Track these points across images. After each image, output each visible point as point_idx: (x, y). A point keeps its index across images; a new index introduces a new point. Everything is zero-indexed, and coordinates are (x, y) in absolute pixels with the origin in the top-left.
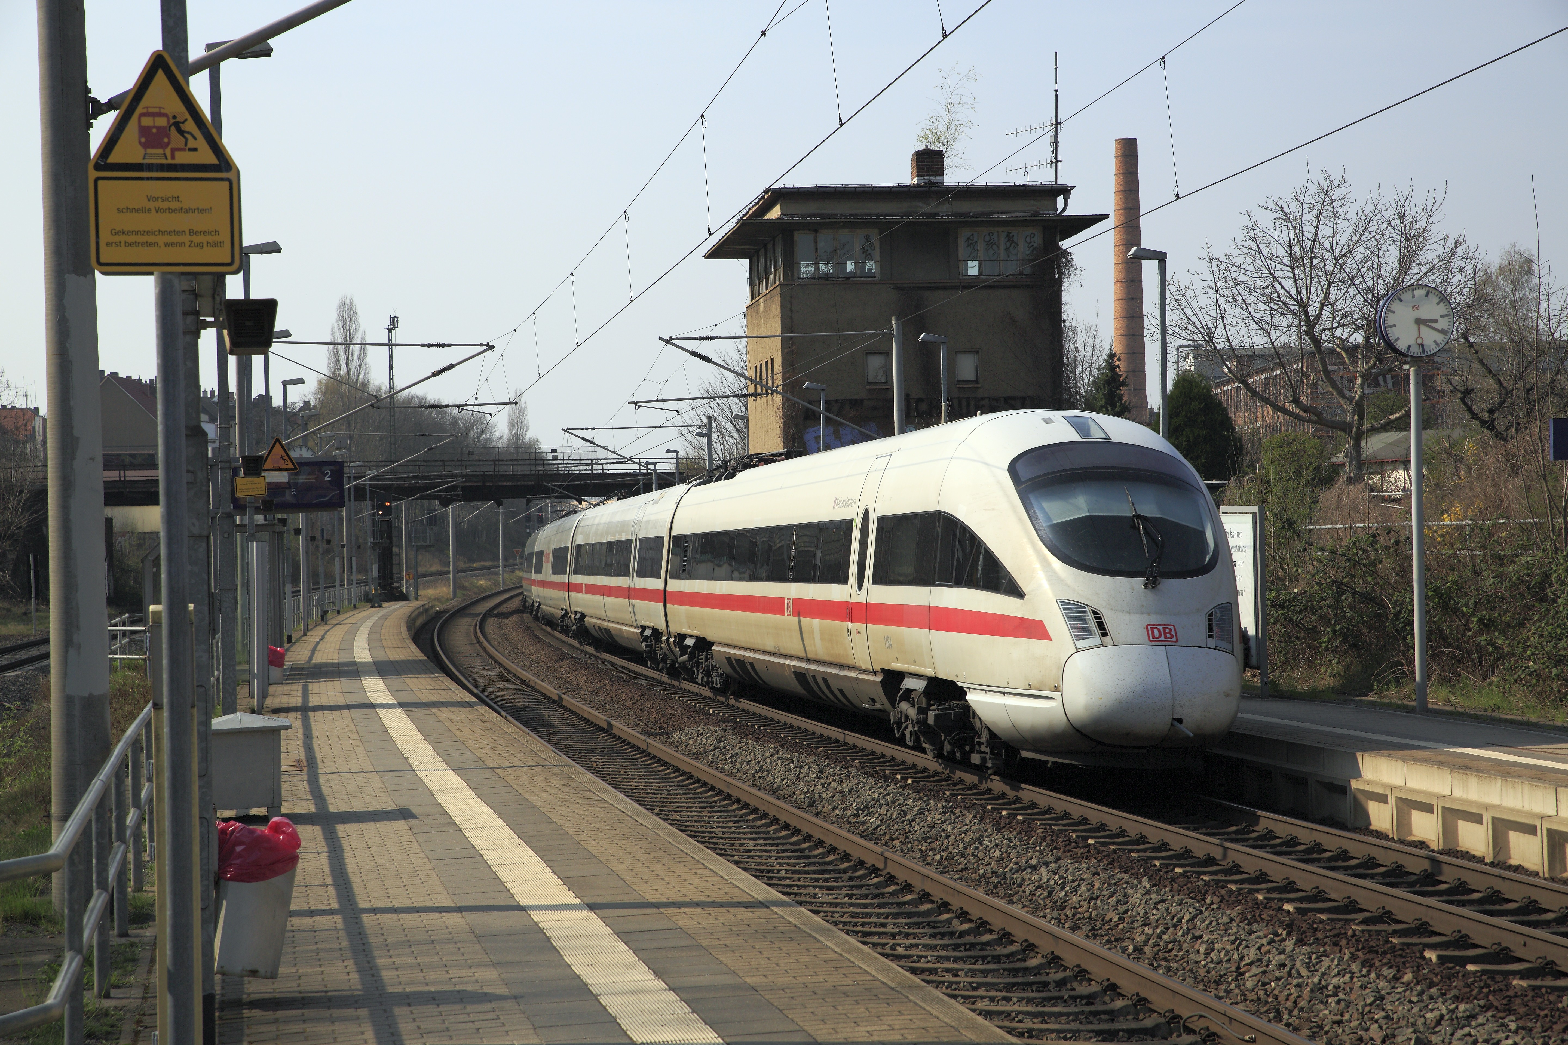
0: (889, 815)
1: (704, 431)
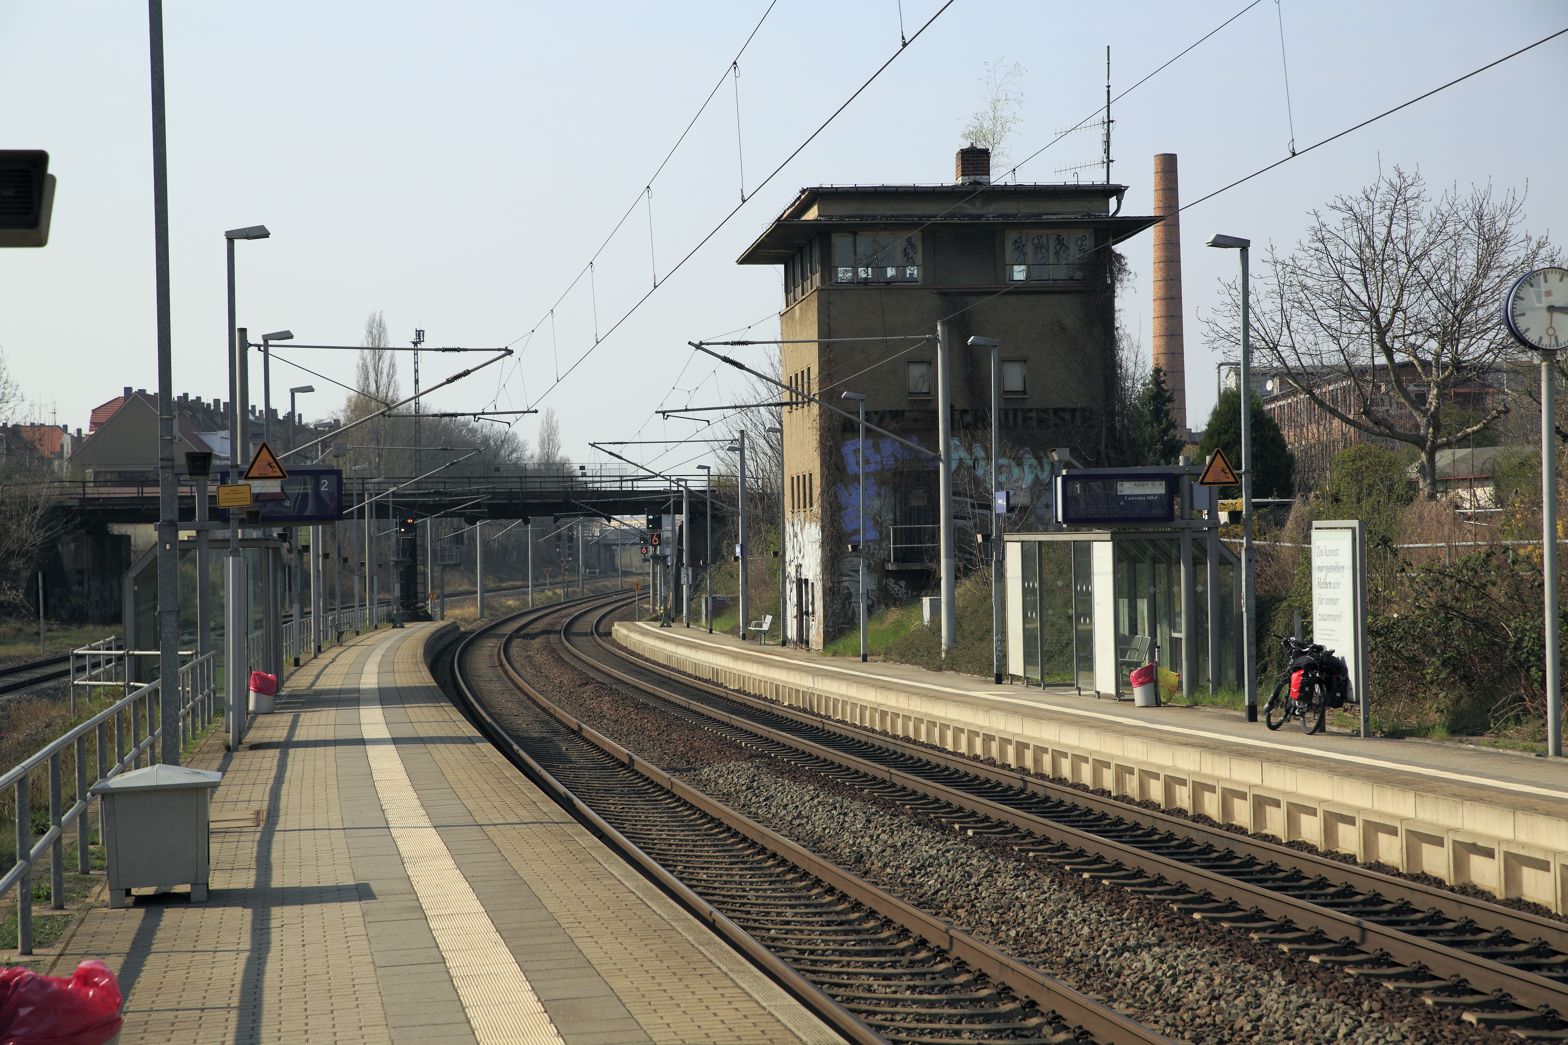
0: (950, 876)
1: (736, 445)
